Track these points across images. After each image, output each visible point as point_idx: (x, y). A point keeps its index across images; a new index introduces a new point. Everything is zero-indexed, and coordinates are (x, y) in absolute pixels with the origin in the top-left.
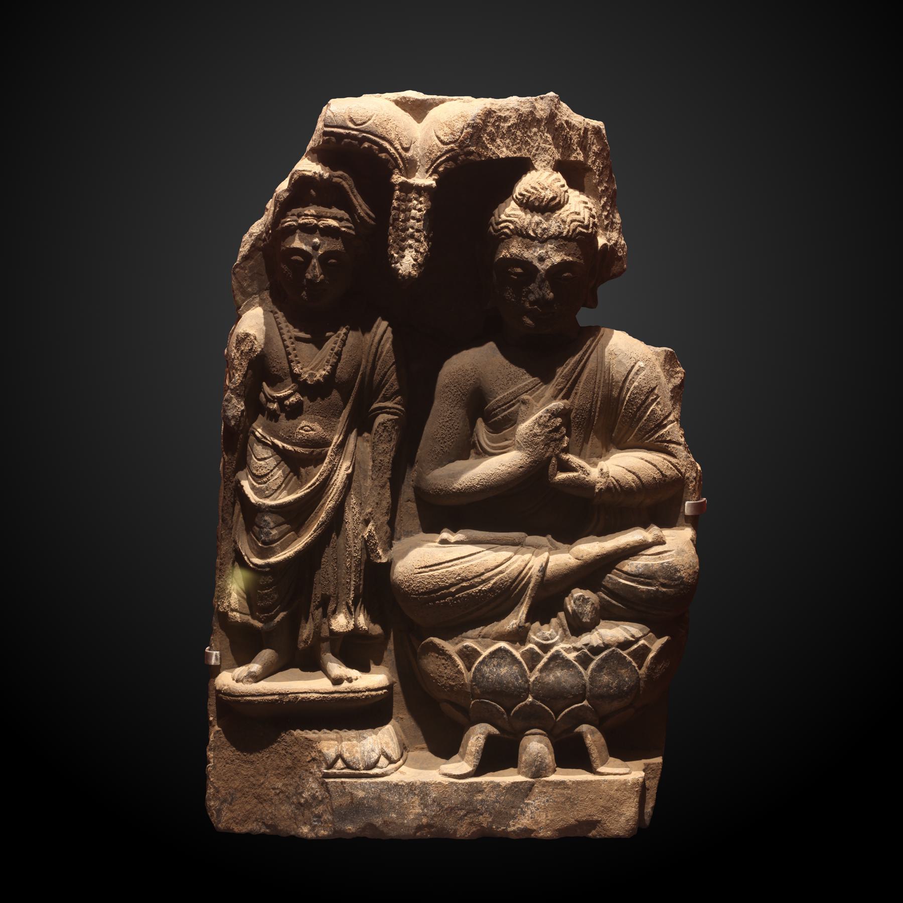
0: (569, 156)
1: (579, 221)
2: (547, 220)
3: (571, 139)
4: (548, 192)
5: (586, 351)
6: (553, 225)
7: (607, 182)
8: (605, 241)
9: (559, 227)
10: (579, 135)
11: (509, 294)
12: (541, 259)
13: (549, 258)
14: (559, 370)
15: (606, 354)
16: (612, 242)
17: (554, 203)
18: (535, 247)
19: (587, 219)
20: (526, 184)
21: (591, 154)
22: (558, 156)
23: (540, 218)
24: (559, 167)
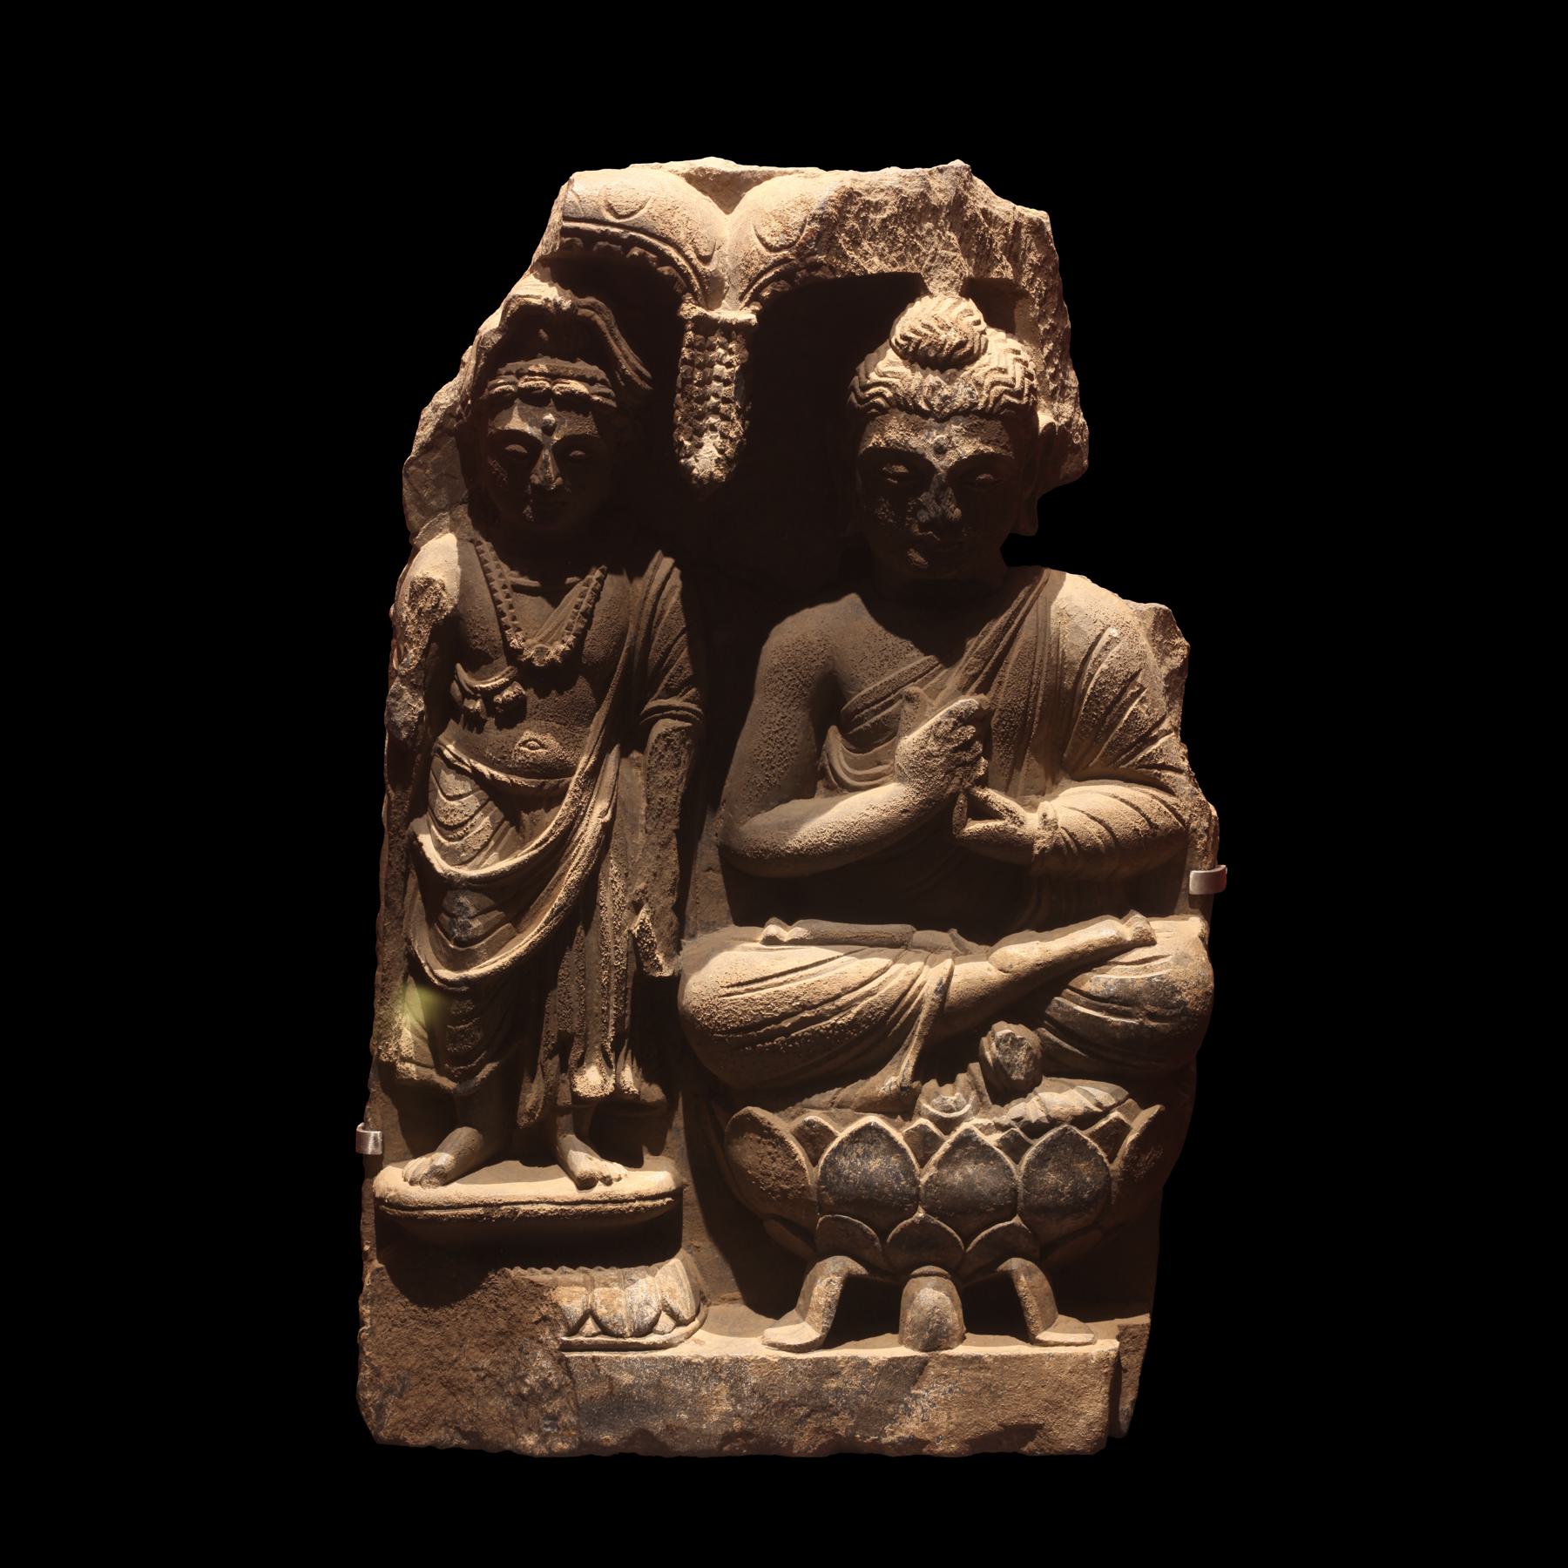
0: (988, 271)
1: (1005, 384)
2: (950, 382)
3: (991, 241)
4: (951, 333)
5: (1018, 609)
6: (960, 391)
7: (1053, 316)
8: (1050, 419)
9: (971, 393)
10: (1006, 234)
11: (884, 511)
12: (940, 450)
13: (954, 447)
14: (971, 643)
15: (1053, 615)
16: (1063, 421)
17: (962, 352)
18: (930, 428)
19: (1018, 380)
20: (913, 319)
21: (1026, 267)
22: (968, 272)
23: (938, 378)
24: (970, 289)
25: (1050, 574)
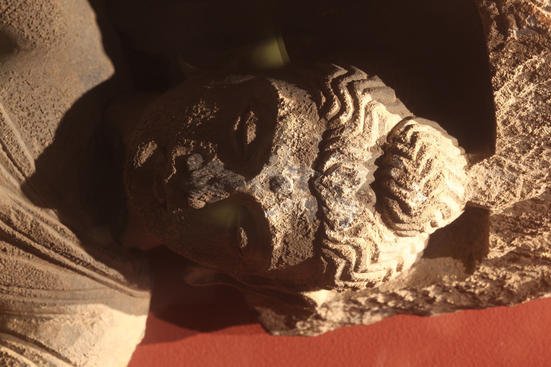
0: (497, 231)
1: (358, 263)
2: (360, 196)
3: (533, 234)
4: (421, 197)
5: (94, 269)
6: (349, 208)
7: (444, 301)
8: (320, 302)
9: (346, 222)
10: (542, 249)
11: (202, 112)
12: (275, 184)
13: (279, 201)
14: (51, 216)
15: (92, 307)
16: (322, 312)
17: (397, 209)
18: (301, 171)
19: (365, 276)
20: (437, 145)
21: (502, 272)
22: (496, 210)
23: (364, 181)
24: (475, 218)
25: (144, 299)
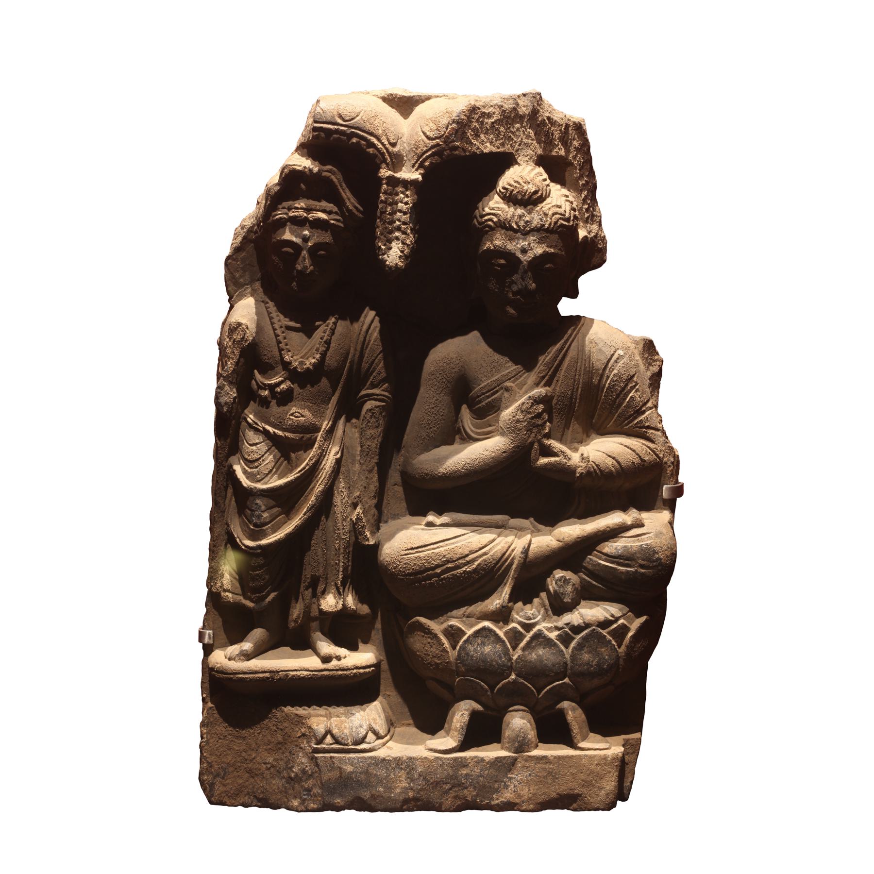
0: (551, 151)
1: (560, 214)
2: (530, 213)
3: (553, 135)
4: (530, 186)
5: (568, 340)
6: (535, 218)
7: (587, 176)
8: (585, 234)
9: (541, 219)
10: (560, 130)
11: (492, 285)
12: (524, 251)
13: (532, 249)
14: (541, 358)
15: (587, 343)
17: (536, 196)
18: (518, 239)
19: (568, 212)
20: (509, 178)
21: (572, 149)
22: (540, 151)
23: (523, 211)
24: (541, 161)
